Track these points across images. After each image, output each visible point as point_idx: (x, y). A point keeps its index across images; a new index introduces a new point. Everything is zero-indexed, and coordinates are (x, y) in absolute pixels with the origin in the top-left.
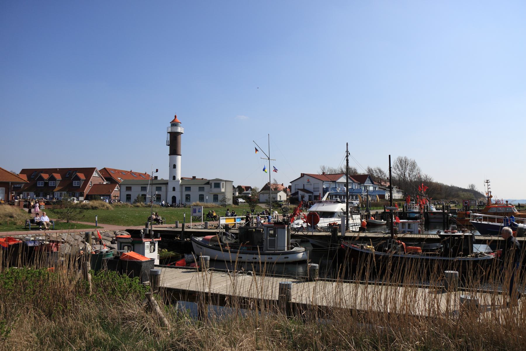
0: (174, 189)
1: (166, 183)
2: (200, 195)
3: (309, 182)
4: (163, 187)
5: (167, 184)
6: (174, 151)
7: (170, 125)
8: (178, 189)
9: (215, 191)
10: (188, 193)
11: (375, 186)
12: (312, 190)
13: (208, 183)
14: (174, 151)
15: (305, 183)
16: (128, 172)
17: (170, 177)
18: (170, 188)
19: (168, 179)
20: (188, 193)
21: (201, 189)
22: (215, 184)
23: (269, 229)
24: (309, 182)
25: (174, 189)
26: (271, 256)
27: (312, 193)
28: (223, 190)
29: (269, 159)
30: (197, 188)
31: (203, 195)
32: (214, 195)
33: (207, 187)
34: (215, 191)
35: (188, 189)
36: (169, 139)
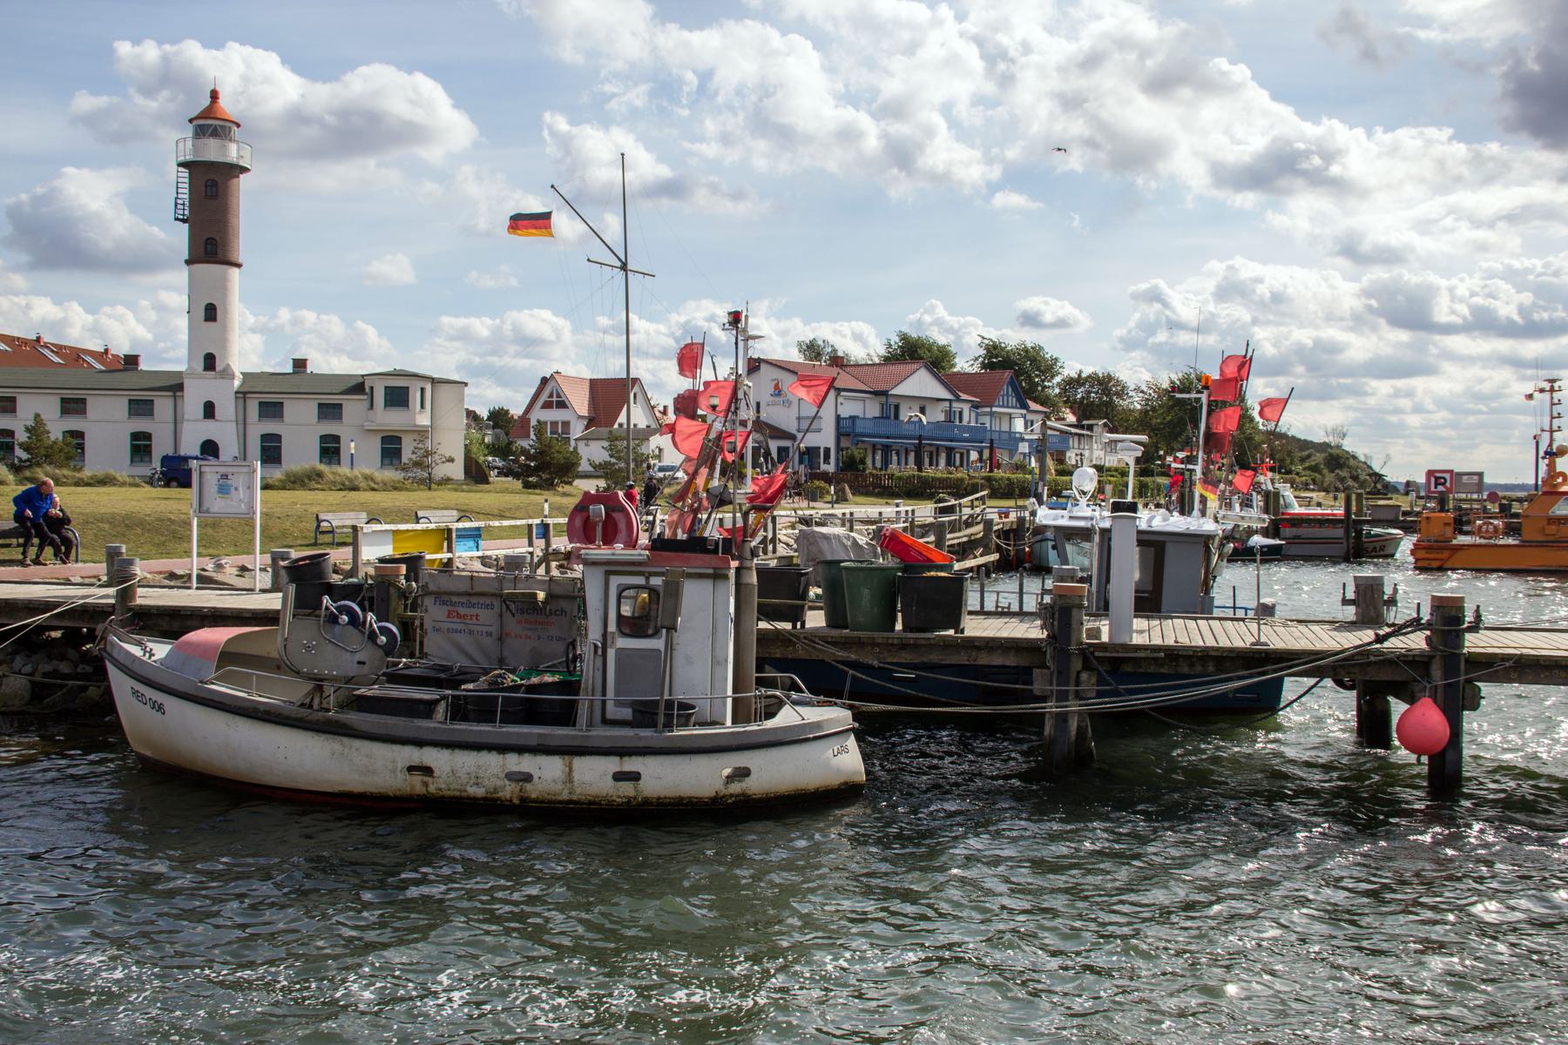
0: (209, 410)
1: (174, 386)
2: (136, 436)
3: (778, 391)
4: (163, 405)
5: (179, 387)
6: (210, 242)
7: (189, 131)
8: (226, 408)
9: (393, 419)
10: (271, 427)
11: (1030, 417)
12: (791, 427)
13: (358, 387)
14: (210, 242)
15: (765, 398)
16: (25, 342)
17: (191, 359)
18: (192, 403)
19: (183, 368)
20: (271, 427)
21: (330, 411)
22: (390, 391)
23: (615, 581)
24: (778, 391)
25: (209, 410)
26: (631, 764)
27: (792, 437)
28: (423, 420)
29: (624, 267)
30: (312, 409)
31: (336, 439)
32: (385, 440)
33: (353, 408)
34: (393, 419)
35: (271, 410)
36: (185, 195)
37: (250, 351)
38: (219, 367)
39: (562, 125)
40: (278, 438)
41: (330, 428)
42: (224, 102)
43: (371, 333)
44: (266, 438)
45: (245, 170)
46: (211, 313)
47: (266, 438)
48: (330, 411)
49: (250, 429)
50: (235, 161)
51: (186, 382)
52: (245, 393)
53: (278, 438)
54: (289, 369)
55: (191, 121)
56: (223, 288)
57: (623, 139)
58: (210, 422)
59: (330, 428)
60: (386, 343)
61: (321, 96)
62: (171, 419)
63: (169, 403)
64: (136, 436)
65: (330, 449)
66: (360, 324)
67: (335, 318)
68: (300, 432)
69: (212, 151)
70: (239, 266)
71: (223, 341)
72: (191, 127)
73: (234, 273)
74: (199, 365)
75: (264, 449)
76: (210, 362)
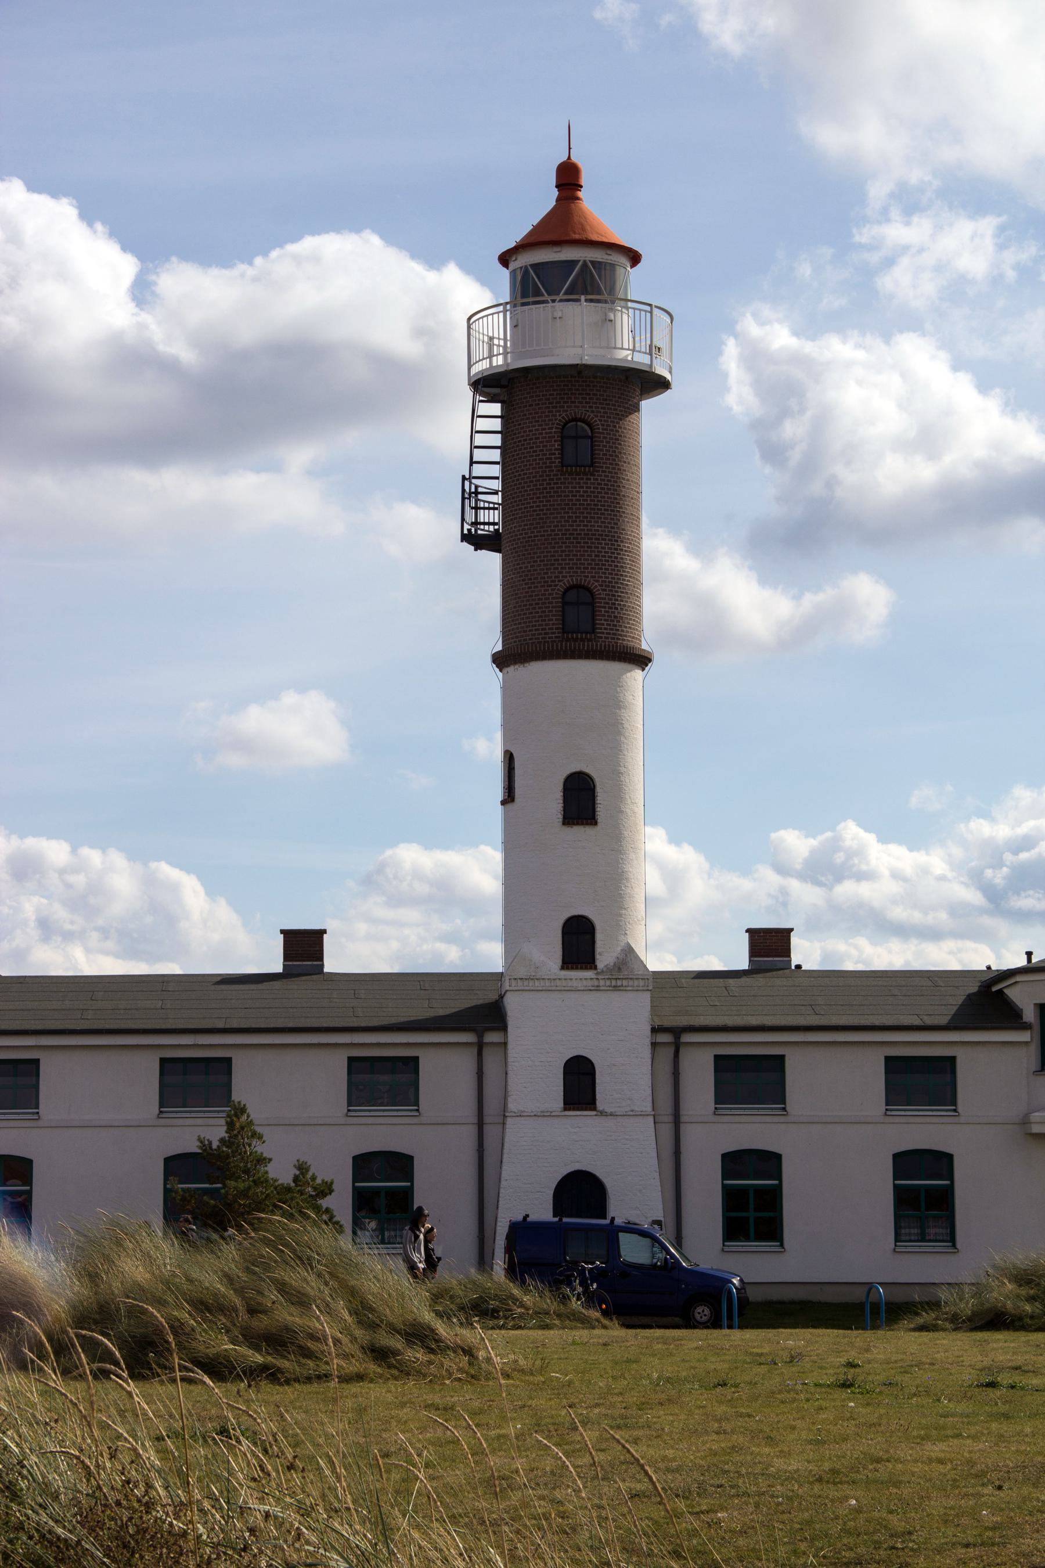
0: (580, 1084)
1: (475, 1013)
2: (907, 1162)
4: (445, 1073)
10: (751, 1130)
20: (751, 1130)
25: (580, 1084)
30: (137, 1078)
35: (752, 1079)
37: (682, 907)
38: (605, 956)
39: (781, 338)
40: (769, 1162)
41: (922, 1130)
42: (591, 200)
43: (191, 891)
44: (735, 1162)
45: (662, 385)
46: (581, 801)
47: (735, 1162)
48: (920, 1081)
49: (691, 1135)
50: (641, 360)
51: (512, 1004)
52: (677, 1032)
53: (769, 1162)
54: (741, 961)
55: (505, 259)
56: (608, 724)
57: (921, 357)
58: (582, 1121)
59: (922, 1130)
60: (224, 912)
61: (207, 298)
62: (467, 1110)
63: (463, 1063)
64: (907, 1162)
65: (924, 1196)
66: (167, 871)
67: (118, 859)
68: (836, 1142)
69: (571, 337)
70: (642, 660)
71: (613, 880)
72: (504, 275)
73: (636, 676)
74: (547, 953)
75: (733, 1199)
76: (579, 942)
